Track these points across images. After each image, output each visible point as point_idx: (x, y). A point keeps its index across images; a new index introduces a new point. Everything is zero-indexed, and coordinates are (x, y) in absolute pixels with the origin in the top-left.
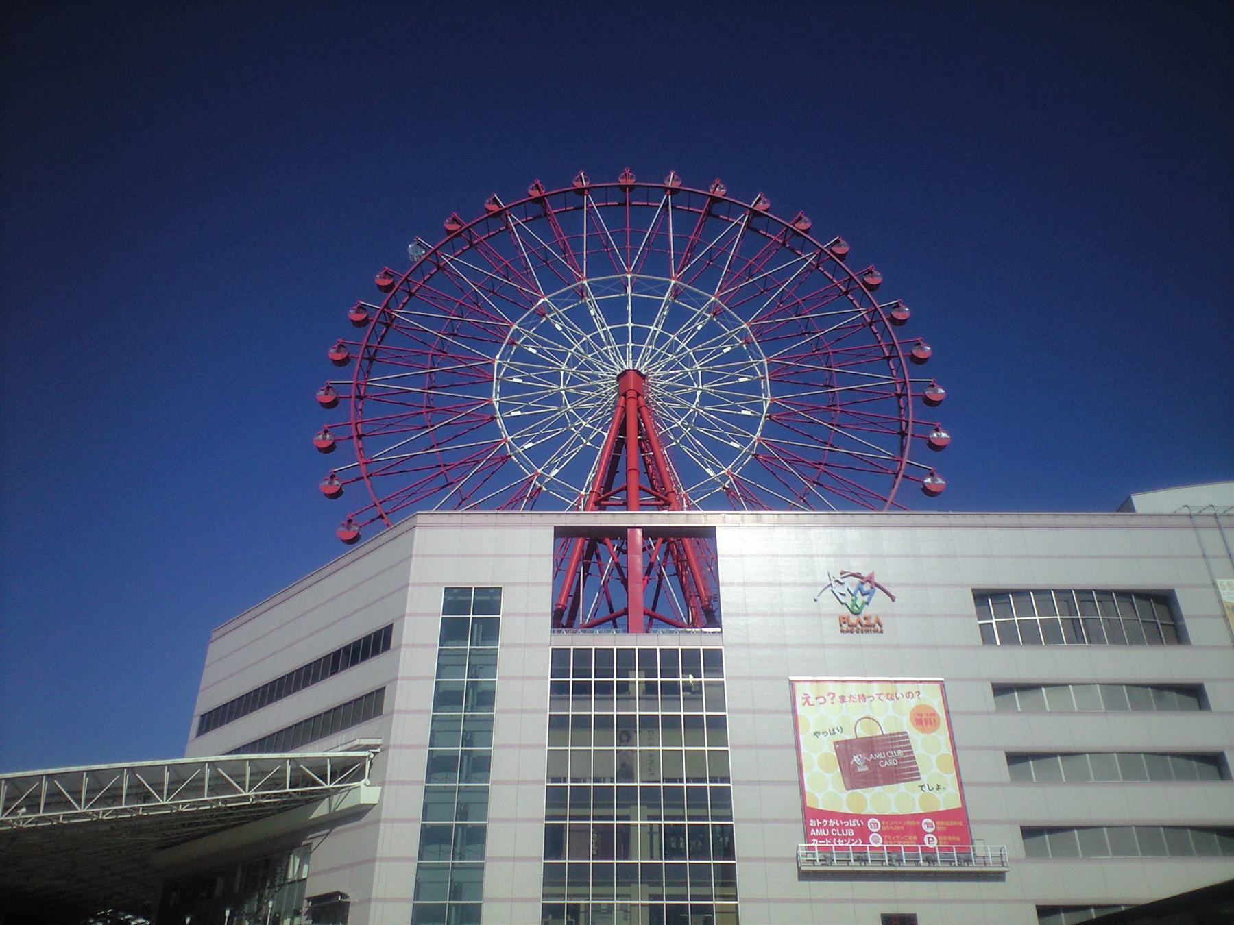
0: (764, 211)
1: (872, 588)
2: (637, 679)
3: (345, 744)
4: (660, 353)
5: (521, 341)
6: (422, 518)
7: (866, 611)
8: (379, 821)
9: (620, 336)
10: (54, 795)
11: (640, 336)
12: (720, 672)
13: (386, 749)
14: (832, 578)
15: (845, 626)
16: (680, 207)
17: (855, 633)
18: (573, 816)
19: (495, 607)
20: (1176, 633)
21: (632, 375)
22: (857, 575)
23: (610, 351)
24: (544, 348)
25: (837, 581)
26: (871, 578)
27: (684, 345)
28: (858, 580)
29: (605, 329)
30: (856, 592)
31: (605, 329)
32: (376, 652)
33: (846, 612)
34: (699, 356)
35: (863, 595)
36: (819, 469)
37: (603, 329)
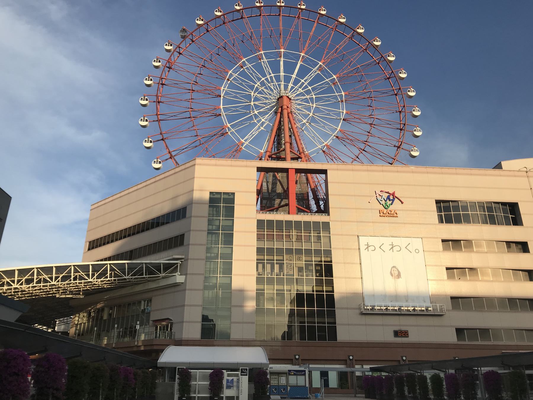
1: (393, 198)
2: (294, 233)
3: (167, 257)
4: (296, 88)
5: (232, 79)
6: (198, 161)
7: (391, 208)
8: (185, 290)
13: (187, 260)
14: (377, 194)
15: (382, 214)
16: (380, 65)
17: (386, 217)
19: (232, 201)
20: (517, 221)
21: (285, 98)
22: (388, 193)
24: (243, 83)
25: (379, 195)
26: (393, 194)
27: (306, 84)
28: (388, 194)
29: (271, 75)
30: (387, 200)
31: (271, 75)
32: (178, 219)
33: (381, 207)
35: (389, 201)
36: (366, 144)
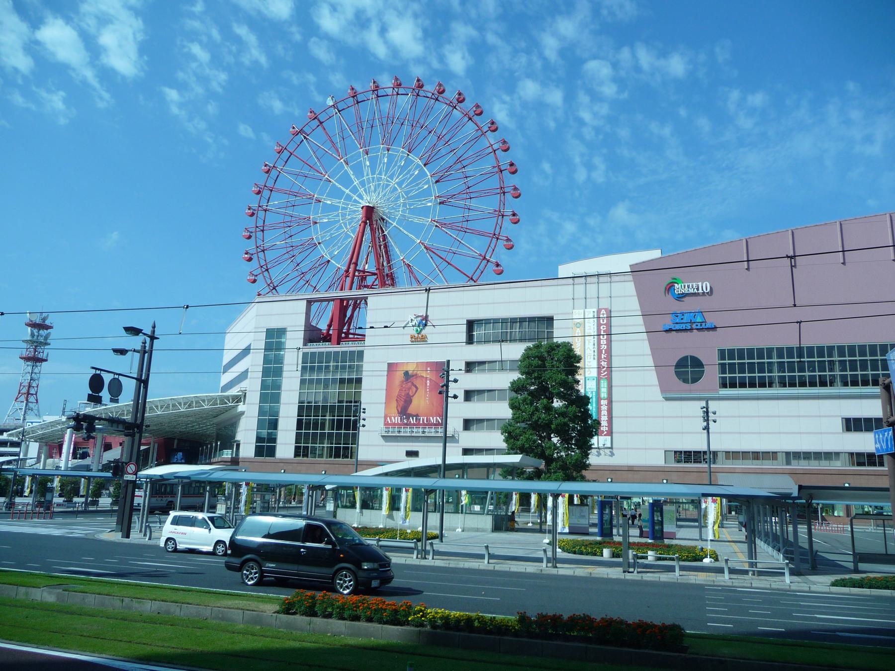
0: (102, 471)
9: (355, 190)
10: (174, 405)
11: (355, 190)
12: (362, 360)
18: (340, 401)
23: (351, 207)
34: (380, 174)
37: (340, 203)
